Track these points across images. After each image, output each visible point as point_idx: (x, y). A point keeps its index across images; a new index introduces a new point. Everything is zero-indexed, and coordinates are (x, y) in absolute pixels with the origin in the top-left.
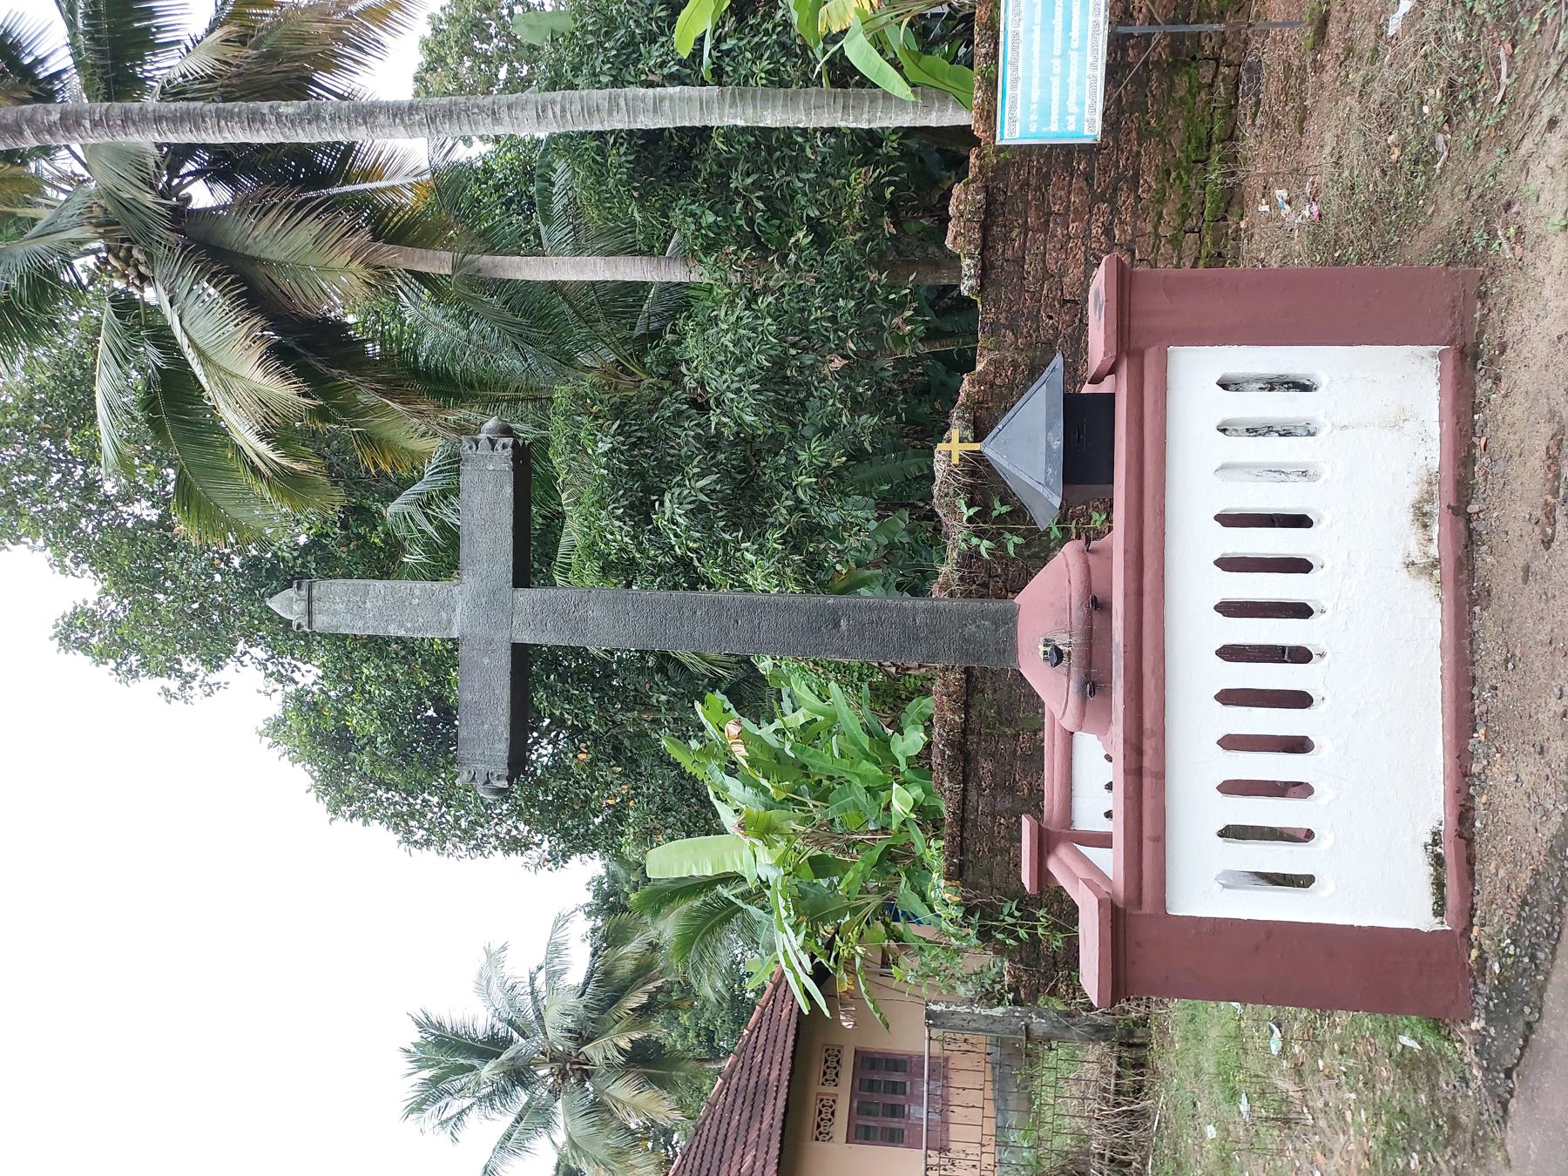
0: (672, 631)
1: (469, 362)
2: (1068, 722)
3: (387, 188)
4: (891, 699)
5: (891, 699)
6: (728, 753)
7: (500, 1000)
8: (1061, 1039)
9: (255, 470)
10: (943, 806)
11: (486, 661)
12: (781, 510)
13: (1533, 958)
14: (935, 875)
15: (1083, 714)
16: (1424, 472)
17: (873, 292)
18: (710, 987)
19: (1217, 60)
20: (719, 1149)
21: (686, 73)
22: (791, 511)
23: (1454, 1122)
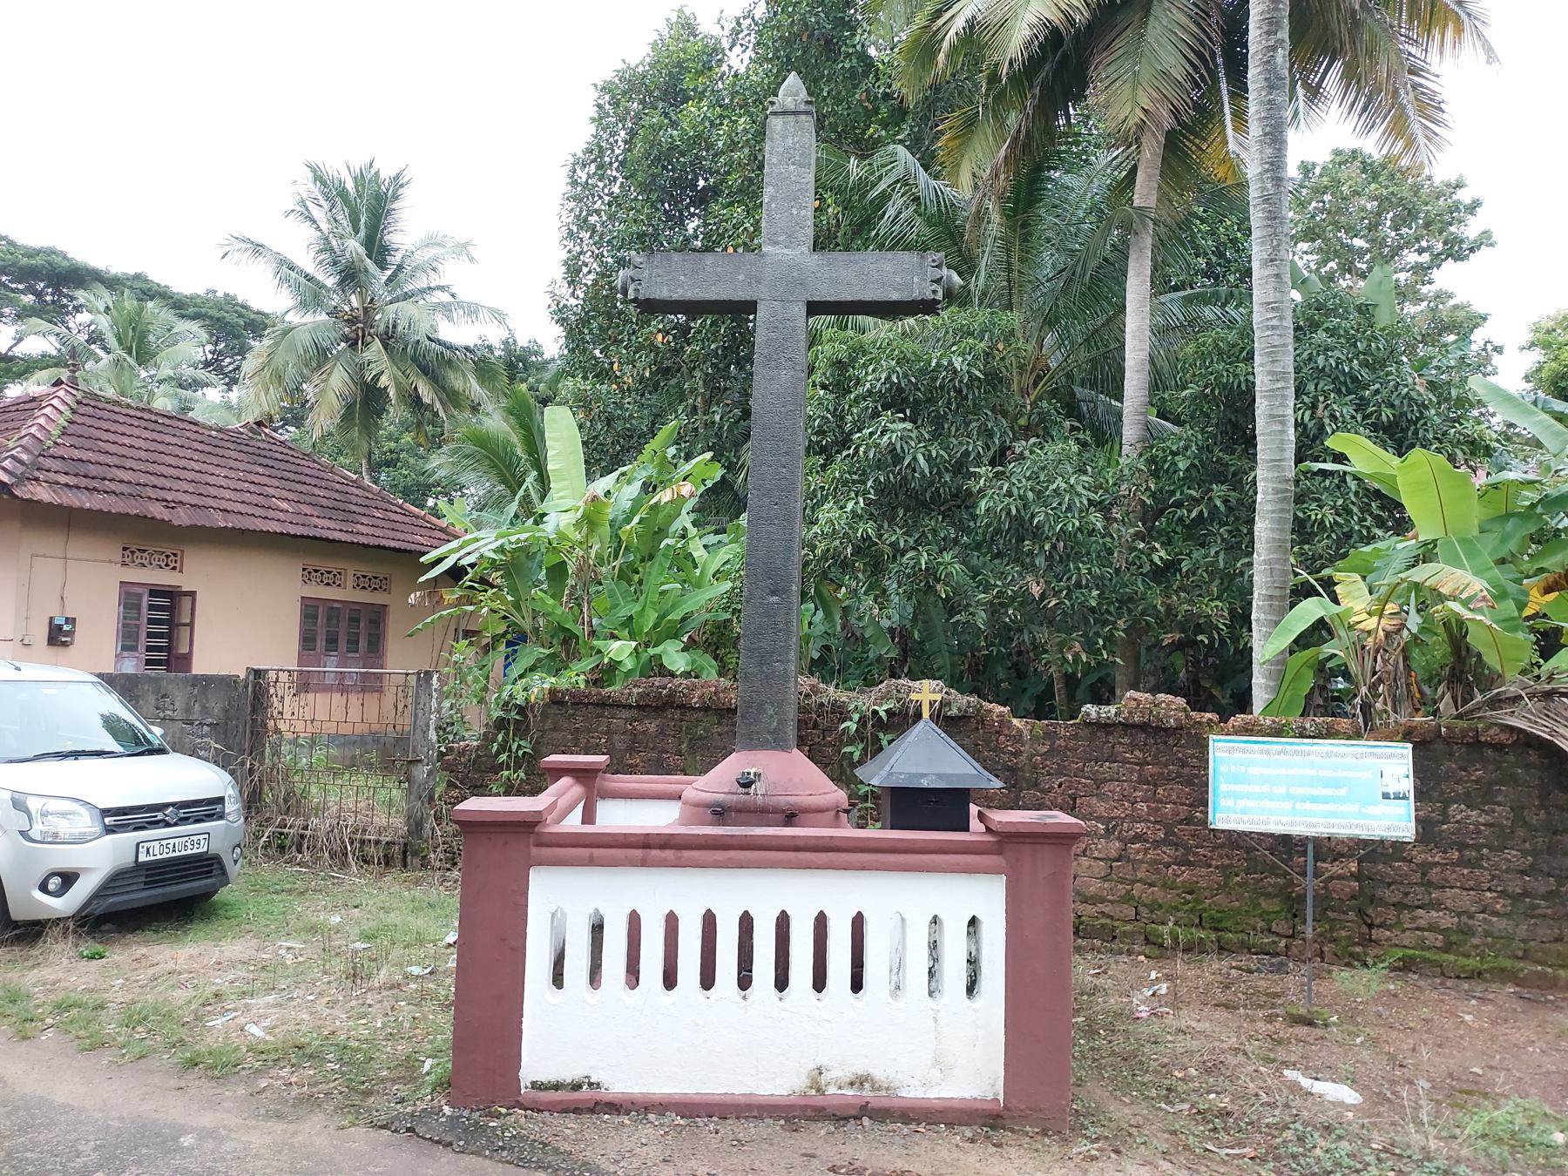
0: (767, 445)
1: (1047, 220)
2: (689, 793)
3: (1225, 136)
4: (716, 640)
5: (716, 640)
6: (664, 484)
7: (420, 257)
8: (409, 790)
9: (938, 14)
10: (616, 687)
11: (741, 277)
12: (896, 535)
13: (503, 1148)
14: (553, 680)
15: (697, 805)
16: (897, 1084)
17: (1105, 623)
18: (439, 464)
19: (1292, 936)
20: (292, 476)
21: (1309, 443)
22: (894, 545)
23: (367, 1094)
